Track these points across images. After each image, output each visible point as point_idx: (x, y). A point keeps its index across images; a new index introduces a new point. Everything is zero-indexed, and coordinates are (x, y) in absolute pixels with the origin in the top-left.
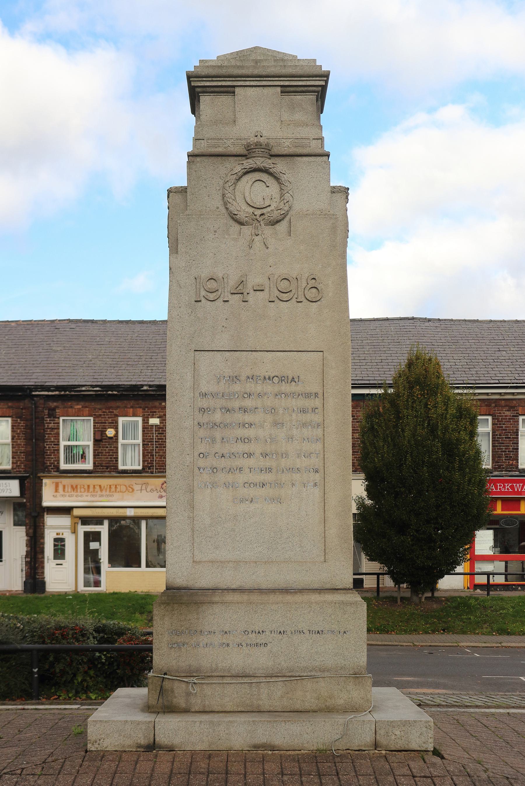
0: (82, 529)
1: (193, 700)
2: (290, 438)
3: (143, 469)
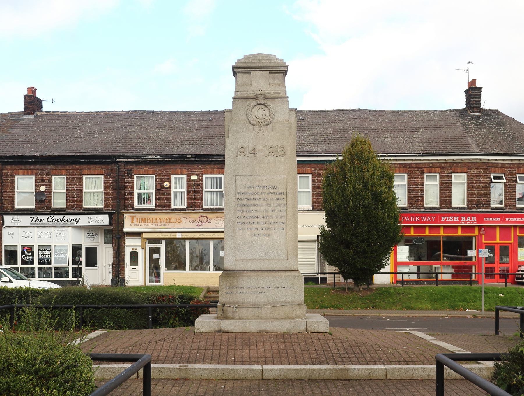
0: (148, 246)
1: (235, 314)
2: (273, 210)
3: (187, 207)
